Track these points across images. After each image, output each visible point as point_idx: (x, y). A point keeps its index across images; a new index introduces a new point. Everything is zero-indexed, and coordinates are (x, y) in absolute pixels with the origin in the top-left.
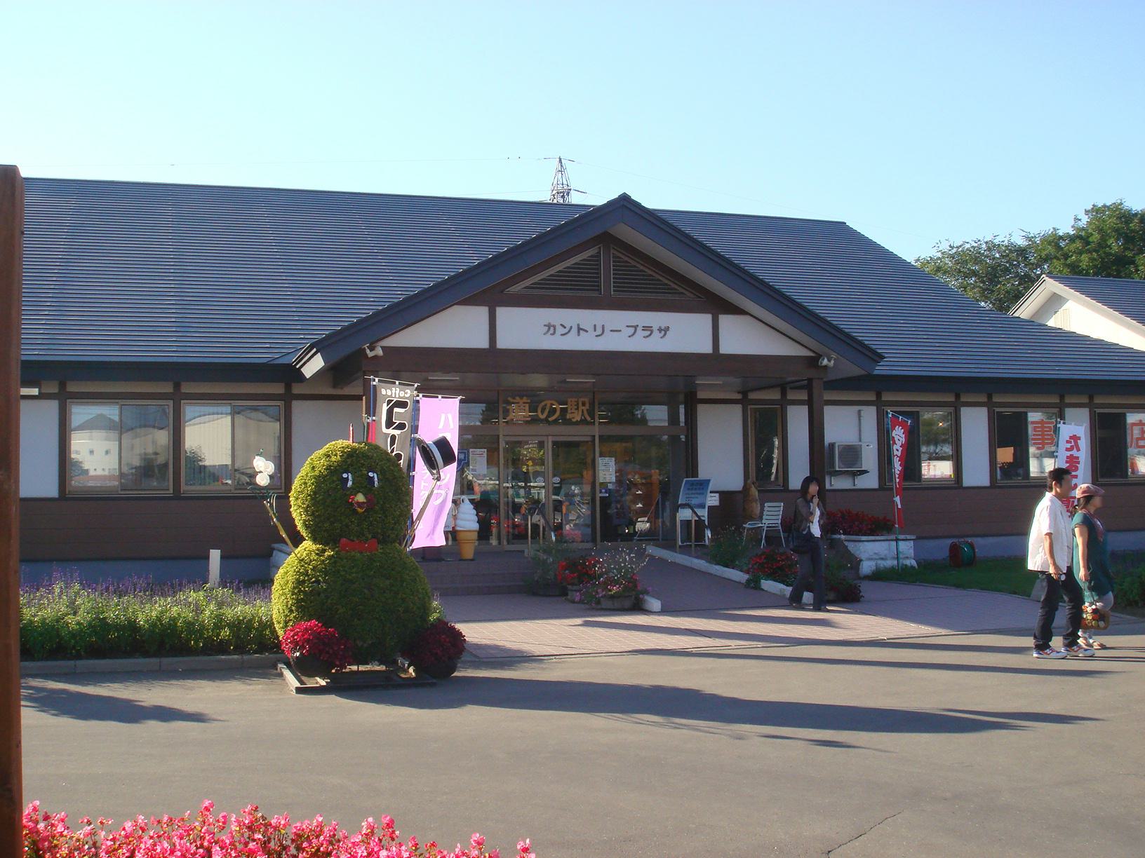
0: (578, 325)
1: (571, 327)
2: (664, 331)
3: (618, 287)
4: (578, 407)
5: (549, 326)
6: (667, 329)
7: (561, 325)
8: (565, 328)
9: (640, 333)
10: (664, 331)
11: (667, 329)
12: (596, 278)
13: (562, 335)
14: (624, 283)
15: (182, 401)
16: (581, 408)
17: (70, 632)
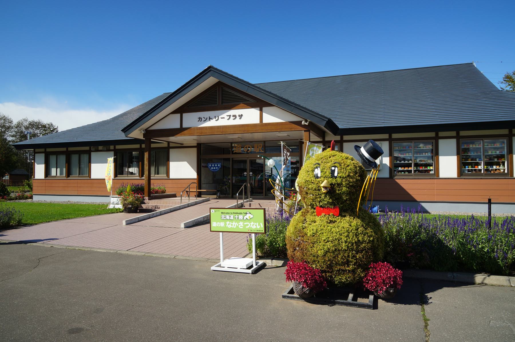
0: (209, 117)
1: (207, 118)
2: (241, 116)
3: (215, 102)
4: (258, 147)
5: (200, 118)
6: (242, 115)
7: (204, 117)
8: (205, 118)
9: (232, 118)
10: (241, 116)
11: (242, 115)
12: (216, 96)
13: (204, 121)
14: (210, 99)
15: (460, 139)
16: (259, 147)
17: (393, 277)
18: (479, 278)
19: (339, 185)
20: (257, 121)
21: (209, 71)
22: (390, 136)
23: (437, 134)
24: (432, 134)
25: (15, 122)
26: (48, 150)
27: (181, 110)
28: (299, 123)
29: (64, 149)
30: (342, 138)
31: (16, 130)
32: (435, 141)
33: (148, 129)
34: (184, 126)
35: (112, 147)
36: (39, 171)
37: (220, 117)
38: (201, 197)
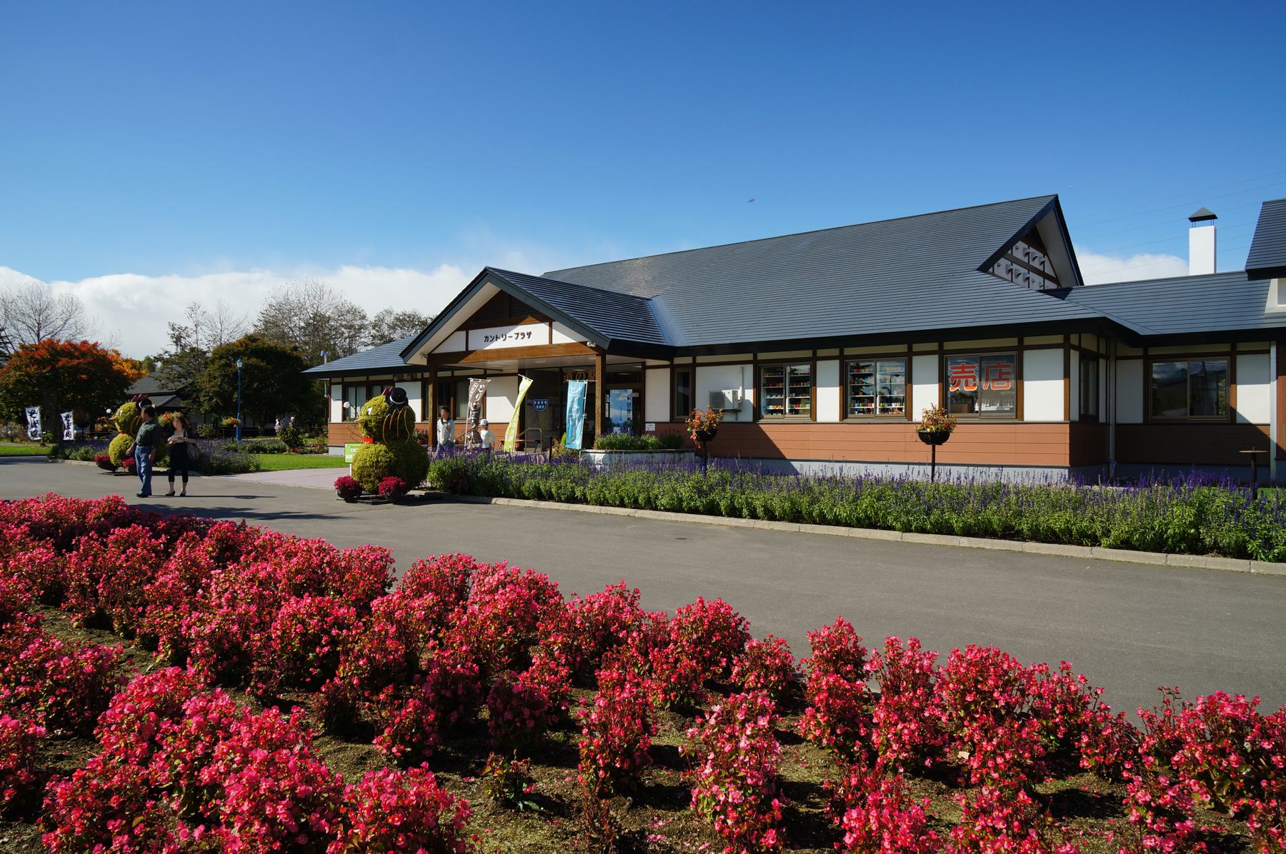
2: (529, 334)
5: (486, 337)
9: (520, 336)
18: (494, 500)
19: (370, 421)
20: (546, 342)
21: (486, 275)
22: (941, 346)
23: (910, 348)
24: (903, 348)
25: (371, 317)
26: (346, 380)
27: (467, 326)
28: (585, 343)
29: (363, 379)
30: (814, 353)
31: (373, 332)
32: (908, 358)
33: (436, 352)
34: (470, 349)
35: (419, 375)
36: (336, 408)
37: (508, 335)
38: (522, 450)
